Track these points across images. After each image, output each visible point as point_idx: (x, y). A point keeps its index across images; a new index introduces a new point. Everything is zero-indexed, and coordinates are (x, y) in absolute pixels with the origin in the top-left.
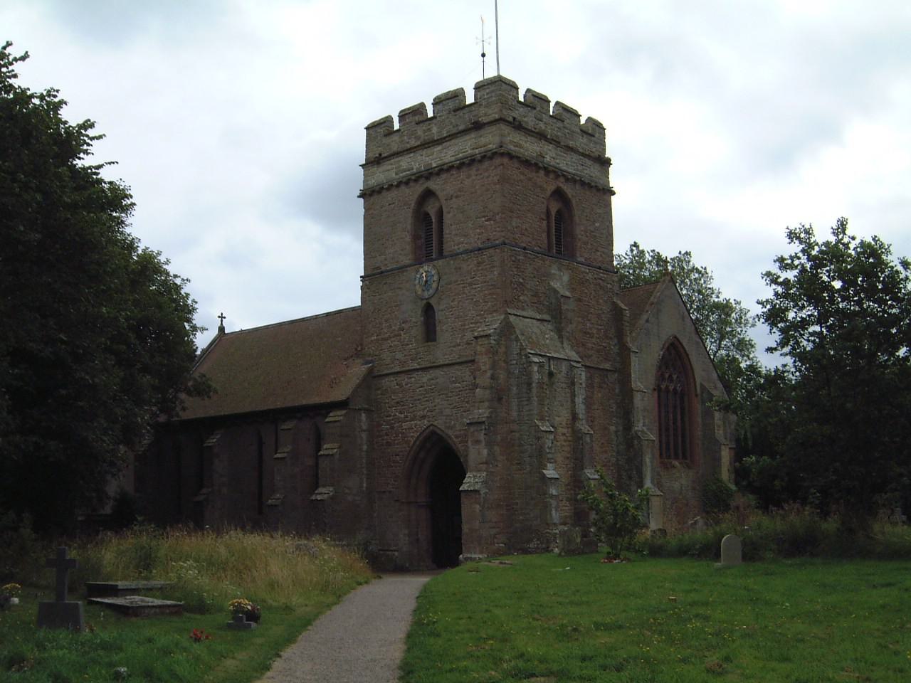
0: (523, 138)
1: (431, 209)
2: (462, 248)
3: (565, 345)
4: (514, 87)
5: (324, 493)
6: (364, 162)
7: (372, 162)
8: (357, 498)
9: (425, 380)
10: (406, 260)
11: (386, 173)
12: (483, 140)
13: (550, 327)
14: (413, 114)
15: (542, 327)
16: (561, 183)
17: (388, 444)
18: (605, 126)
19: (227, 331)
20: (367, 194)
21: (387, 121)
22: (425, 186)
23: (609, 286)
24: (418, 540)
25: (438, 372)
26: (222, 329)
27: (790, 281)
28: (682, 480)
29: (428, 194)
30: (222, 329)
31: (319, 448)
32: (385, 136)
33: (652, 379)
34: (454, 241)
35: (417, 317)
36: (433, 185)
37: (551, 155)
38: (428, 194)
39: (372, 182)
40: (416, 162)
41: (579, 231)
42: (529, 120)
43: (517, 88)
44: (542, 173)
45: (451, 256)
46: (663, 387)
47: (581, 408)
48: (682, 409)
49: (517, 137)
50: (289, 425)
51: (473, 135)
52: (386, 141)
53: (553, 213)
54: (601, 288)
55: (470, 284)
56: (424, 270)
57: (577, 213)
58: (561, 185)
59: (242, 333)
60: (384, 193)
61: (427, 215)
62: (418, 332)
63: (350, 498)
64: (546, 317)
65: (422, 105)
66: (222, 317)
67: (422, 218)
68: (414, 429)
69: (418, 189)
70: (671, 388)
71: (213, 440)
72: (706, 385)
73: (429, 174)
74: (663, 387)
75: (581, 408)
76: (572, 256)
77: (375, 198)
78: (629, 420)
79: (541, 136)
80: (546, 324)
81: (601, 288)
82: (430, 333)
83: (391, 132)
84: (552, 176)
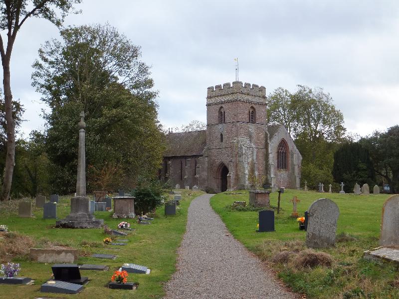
1: (222, 110)
5: (197, 176)
7: (209, 98)
10: (217, 123)
11: (213, 101)
14: (218, 87)
20: (208, 105)
21: (213, 88)
27: (311, 267)
28: (283, 174)
29: (222, 107)
31: (196, 165)
33: (275, 150)
34: (227, 120)
35: (219, 136)
37: (250, 98)
38: (222, 107)
40: (219, 99)
41: (257, 116)
42: (245, 91)
43: (242, 83)
48: (285, 157)
50: (189, 159)
56: (220, 126)
57: (256, 110)
65: (221, 85)
67: (220, 113)
68: (218, 162)
69: (220, 106)
71: (170, 162)
73: (222, 103)
79: (248, 94)
82: (222, 141)
83: (213, 91)
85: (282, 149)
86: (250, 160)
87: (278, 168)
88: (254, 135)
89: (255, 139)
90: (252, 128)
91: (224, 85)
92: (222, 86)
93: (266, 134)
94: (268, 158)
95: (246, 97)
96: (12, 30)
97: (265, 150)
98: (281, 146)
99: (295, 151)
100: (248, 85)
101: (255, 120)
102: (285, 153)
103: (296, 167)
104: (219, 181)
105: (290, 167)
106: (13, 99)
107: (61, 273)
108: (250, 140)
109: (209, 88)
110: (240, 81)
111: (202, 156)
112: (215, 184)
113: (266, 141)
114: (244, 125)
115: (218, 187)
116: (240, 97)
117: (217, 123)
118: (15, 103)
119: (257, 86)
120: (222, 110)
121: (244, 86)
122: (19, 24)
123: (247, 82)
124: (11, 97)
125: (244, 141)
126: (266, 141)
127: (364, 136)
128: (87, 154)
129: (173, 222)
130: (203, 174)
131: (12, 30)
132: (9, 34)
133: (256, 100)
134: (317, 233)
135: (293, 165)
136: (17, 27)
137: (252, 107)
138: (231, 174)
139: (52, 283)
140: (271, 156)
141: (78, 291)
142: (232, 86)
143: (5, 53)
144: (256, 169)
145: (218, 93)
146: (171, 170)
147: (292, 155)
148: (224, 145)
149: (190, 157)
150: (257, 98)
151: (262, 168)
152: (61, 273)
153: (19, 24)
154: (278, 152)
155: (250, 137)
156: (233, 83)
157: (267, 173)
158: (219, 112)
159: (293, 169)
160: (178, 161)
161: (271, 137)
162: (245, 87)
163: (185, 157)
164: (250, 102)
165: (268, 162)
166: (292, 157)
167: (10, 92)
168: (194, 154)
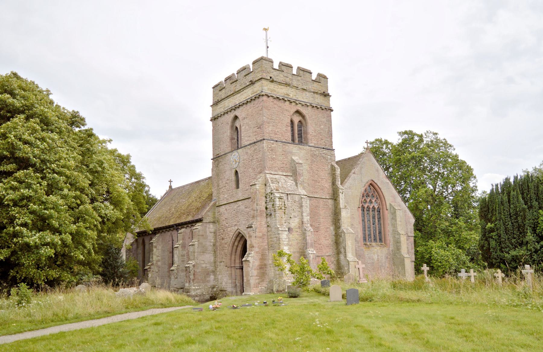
0: (276, 87)
1: (237, 124)
2: (248, 143)
3: (299, 188)
6: (212, 104)
8: (207, 265)
9: (235, 207)
11: (221, 108)
12: (255, 89)
13: (291, 178)
15: (286, 179)
16: (299, 108)
17: (223, 239)
18: (328, 77)
19: (173, 187)
22: (234, 114)
23: (329, 157)
24: (236, 285)
25: (240, 203)
26: (170, 187)
28: (378, 253)
29: (236, 117)
30: (170, 187)
32: (220, 90)
33: (356, 203)
34: (245, 140)
36: (237, 113)
37: (292, 94)
38: (236, 117)
39: (215, 114)
42: (280, 77)
44: (287, 103)
45: (245, 147)
46: (366, 206)
47: (306, 218)
48: (379, 218)
49: (272, 86)
51: (252, 87)
52: (220, 93)
54: (324, 158)
55: (251, 160)
56: (235, 155)
58: (299, 109)
59: (179, 188)
60: (219, 118)
61: (237, 128)
62: (234, 185)
63: (204, 266)
64: (289, 174)
66: (170, 181)
68: (231, 232)
69: (231, 115)
70: (371, 207)
72: (393, 204)
74: (366, 206)
75: (306, 218)
76: (306, 144)
77: (216, 121)
78: (335, 224)
79: (287, 85)
80: (289, 177)
81: (324, 158)
82: (238, 187)
84: (293, 104)
85: (371, 202)
86: (294, 223)
87: (365, 240)
90: (298, 154)
94: (339, 220)
95: (281, 91)
97: (331, 202)
98: (368, 196)
99: (399, 206)
100: (285, 67)
103: (403, 239)
105: (390, 238)
108: (296, 181)
110: (269, 57)
111: (200, 220)
113: (334, 183)
114: (279, 147)
116: (267, 87)
120: (237, 124)
126: (334, 183)
127: (531, 170)
135: (396, 232)
137: (298, 112)
140: (344, 214)
144: (18, 324)
147: (394, 213)
151: (327, 240)
154: (363, 208)
156: (254, 63)
157: (338, 253)
158: (232, 126)
159: (397, 243)
162: (280, 70)
164: (296, 102)
165: (339, 228)
166: (394, 218)
168: (190, 218)
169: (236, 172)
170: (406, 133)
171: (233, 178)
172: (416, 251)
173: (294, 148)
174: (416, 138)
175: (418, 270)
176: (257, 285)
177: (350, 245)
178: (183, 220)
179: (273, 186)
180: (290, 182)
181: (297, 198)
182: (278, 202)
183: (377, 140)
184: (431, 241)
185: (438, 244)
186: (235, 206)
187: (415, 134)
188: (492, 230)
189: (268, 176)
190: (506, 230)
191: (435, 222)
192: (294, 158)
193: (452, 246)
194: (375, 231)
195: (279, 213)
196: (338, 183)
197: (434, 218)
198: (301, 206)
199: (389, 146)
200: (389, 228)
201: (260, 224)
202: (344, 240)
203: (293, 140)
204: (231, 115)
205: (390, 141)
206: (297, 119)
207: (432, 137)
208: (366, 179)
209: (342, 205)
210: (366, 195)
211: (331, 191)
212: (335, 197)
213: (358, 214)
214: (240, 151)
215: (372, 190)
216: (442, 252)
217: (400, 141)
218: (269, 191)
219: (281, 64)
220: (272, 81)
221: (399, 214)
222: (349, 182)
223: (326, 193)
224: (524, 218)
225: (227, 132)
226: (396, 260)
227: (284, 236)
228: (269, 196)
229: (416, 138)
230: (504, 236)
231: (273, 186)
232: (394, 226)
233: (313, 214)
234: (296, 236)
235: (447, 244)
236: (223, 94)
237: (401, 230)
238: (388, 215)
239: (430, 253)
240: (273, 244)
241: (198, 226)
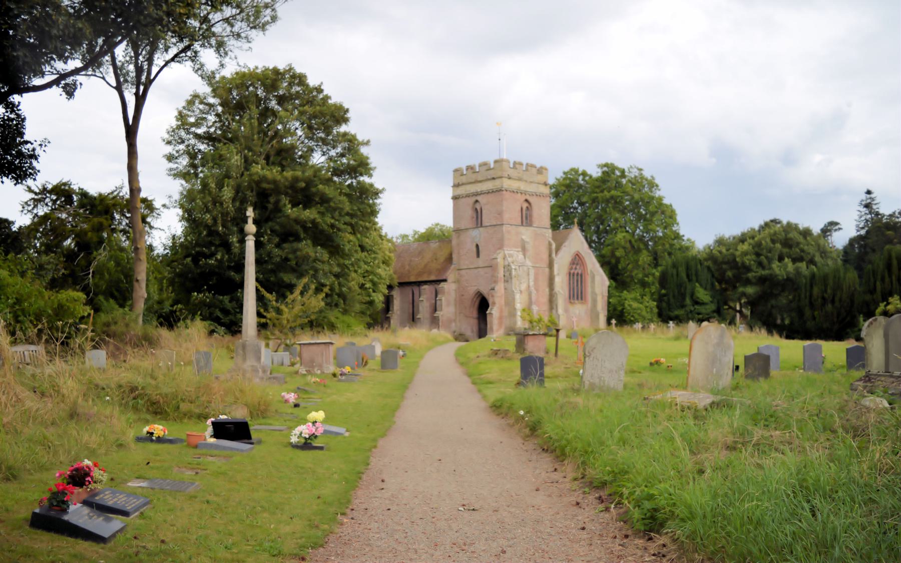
4: (508, 162)
7: (456, 186)
11: (461, 191)
14: (470, 168)
20: (455, 198)
28: (579, 309)
29: (477, 201)
36: (479, 198)
37: (523, 186)
38: (477, 201)
42: (513, 173)
47: (532, 283)
53: (524, 208)
56: (475, 233)
62: (475, 255)
68: (472, 291)
69: (474, 199)
73: (477, 194)
79: (520, 179)
82: (478, 255)
83: (462, 175)
86: (524, 287)
88: (529, 247)
89: (530, 252)
90: (526, 234)
91: (480, 166)
92: (465, 169)
93: (550, 244)
96: (142, 88)
98: (573, 264)
101: (531, 221)
102: (581, 275)
104: (474, 322)
106: (143, 195)
107: (223, 430)
108: (524, 255)
109: (456, 171)
111: (445, 280)
112: (469, 326)
113: (550, 255)
115: (472, 332)
117: (471, 226)
118: (144, 201)
119: (533, 166)
121: (512, 166)
122: (152, 77)
123: (469, 164)
124: (139, 190)
125: (512, 255)
126: (550, 255)
128: (259, 262)
129: (393, 376)
130: (447, 310)
131: (142, 88)
132: (137, 94)
133: (532, 188)
134: (597, 381)
135: (594, 294)
136: (149, 82)
137: (526, 201)
138: (494, 312)
139: (213, 440)
141: (246, 451)
142: (492, 166)
143: (131, 122)
145: (473, 177)
146: (397, 304)
148: (480, 262)
149: (426, 282)
150: (534, 185)
151: (545, 299)
152: (223, 430)
153: (152, 77)
154: (570, 274)
155: (524, 250)
159: (595, 301)
160: (408, 290)
161: (558, 249)
163: (419, 284)
167: (138, 181)
168: (433, 278)
169: (477, 246)
170: (606, 165)
171: (475, 249)
172: (609, 303)
173: (523, 229)
174: (618, 173)
175: (609, 323)
176: (497, 331)
177: (561, 302)
178: (425, 278)
179: (510, 260)
180: (521, 256)
181: (525, 268)
182: (514, 273)
183: (572, 170)
184: (625, 292)
185: (632, 295)
186: (476, 271)
187: (617, 168)
188: (665, 295)
189: (506, 252)
190: (674, 296)
191: (631, 272)
192: (524, 237)
193: (647, 298)
194: (577, 292)
195: (514, 280)
196: (554, 255)
197: (630, 267)
198: (528, 275)
199: (587, 178)
200: (589, 290)
201: (500, 287)
202: (557, 299)
203: (522, 222)
204: (474, 199)
205: (589, 173)
206: (525, 205)
207: (635, 173)
208: (573, 251)
209: (556, 272)
210: (573, 263)
211: (547, 262)
212: (551, 265)
213: (566, 279)
214: (481, 229)
215: (577, 260)
216: (635, 305)
217: (600, 174)
218: (507, 263)
219: (515, 163)
220: (510, 178)
221: (597, 278)
222: (561, 254)
223: (544, 264)
224: (686, 288)
225: (469, 213)
226: (594, 316)
227: (518, 296)
228: (507, 268)
229: (618, 173)
230: (672, 300)
231: (510, 260)
232: (593, 287)
233: (536, 280)
234: (525, 296)
235: (642, 296)
236: (464, 179)
237: (598, 290)
238: (589, 280)
239: (623, 305)
240: (510, 302)
241: (442, 284)
